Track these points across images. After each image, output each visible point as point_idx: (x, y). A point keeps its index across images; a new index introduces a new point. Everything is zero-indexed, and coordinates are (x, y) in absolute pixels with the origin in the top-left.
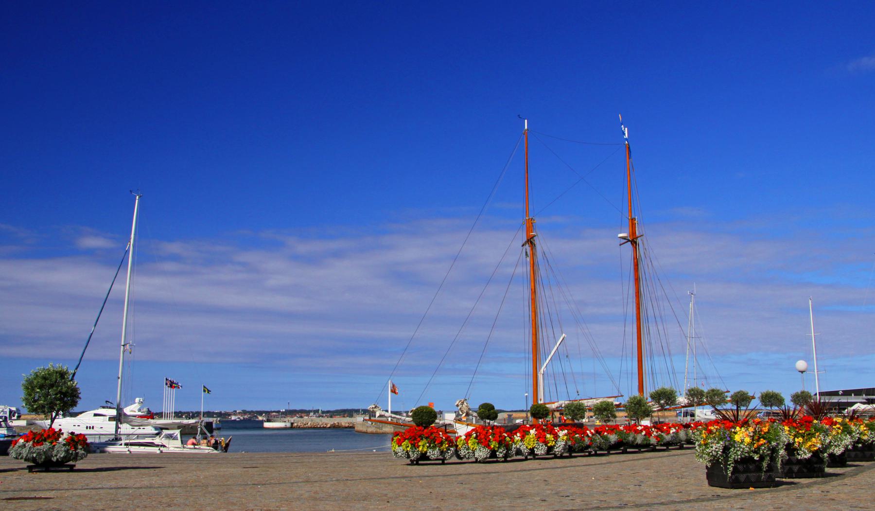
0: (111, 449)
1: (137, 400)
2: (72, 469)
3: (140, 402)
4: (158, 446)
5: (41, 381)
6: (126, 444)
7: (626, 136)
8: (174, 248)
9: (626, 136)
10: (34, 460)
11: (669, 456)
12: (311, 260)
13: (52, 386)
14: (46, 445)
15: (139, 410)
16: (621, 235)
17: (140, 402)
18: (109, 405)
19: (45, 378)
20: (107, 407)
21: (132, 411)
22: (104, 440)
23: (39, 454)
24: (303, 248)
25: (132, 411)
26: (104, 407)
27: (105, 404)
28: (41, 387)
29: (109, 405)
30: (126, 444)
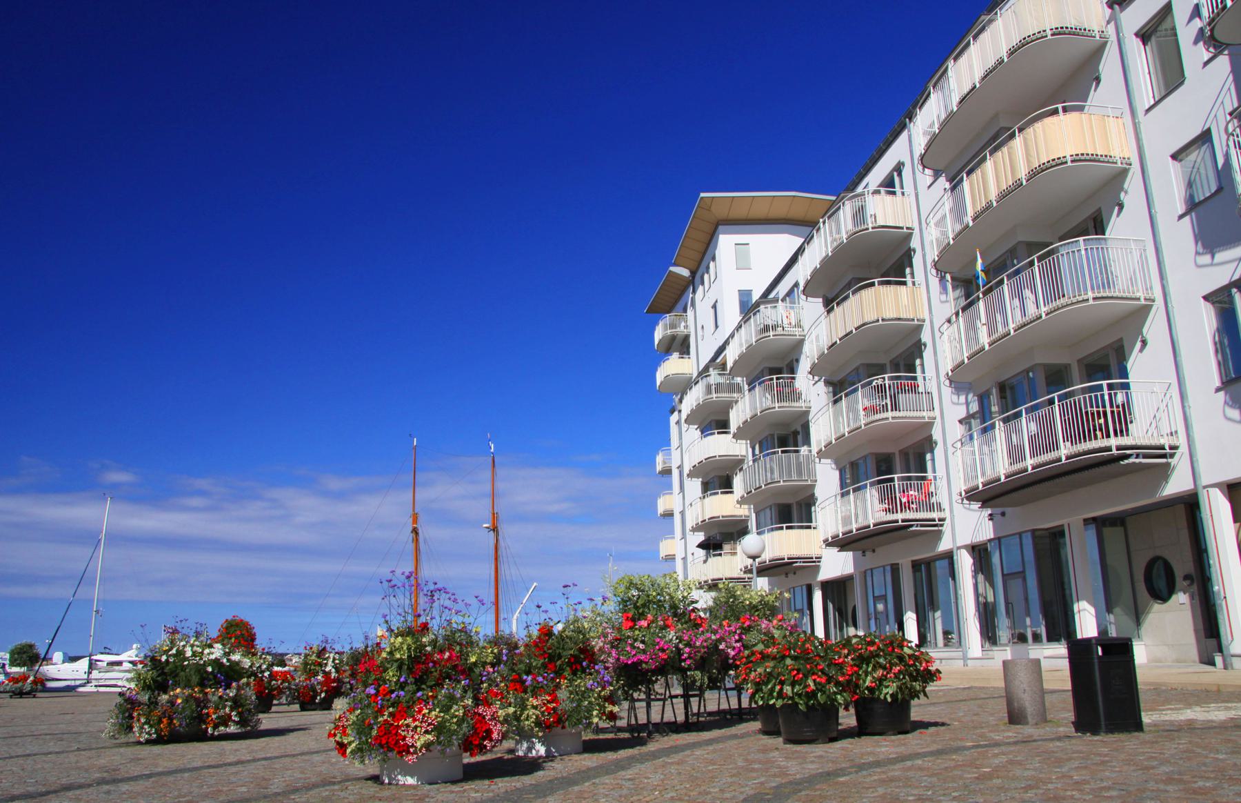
0: (81, 689)
1: (135, 646)
2: (34, 696)
3: (137, 649)
4: (120, 687)
5: (18, 650)
6: (96, 686)
7: (492, 450)
8: (203, 483)
9: (492, 450)
10: (13, 692)
11: (75, 680)
12: (340, 496)
13: (24, 653)
14: (20, 684)
15: (137, 656)
16: (485, 526)
17: (137, 649)
18: (107, 651)
19: (20, 649)
20: (106, 653)
21: (130, 656)
22: (78, 683)
23: (16, 689)
24: (334, 483)
25: (130, 656)
26: (102, 653)
27: (103, 651)
28: (18, 653)
29: (107, 651)
30: (96, 686)
